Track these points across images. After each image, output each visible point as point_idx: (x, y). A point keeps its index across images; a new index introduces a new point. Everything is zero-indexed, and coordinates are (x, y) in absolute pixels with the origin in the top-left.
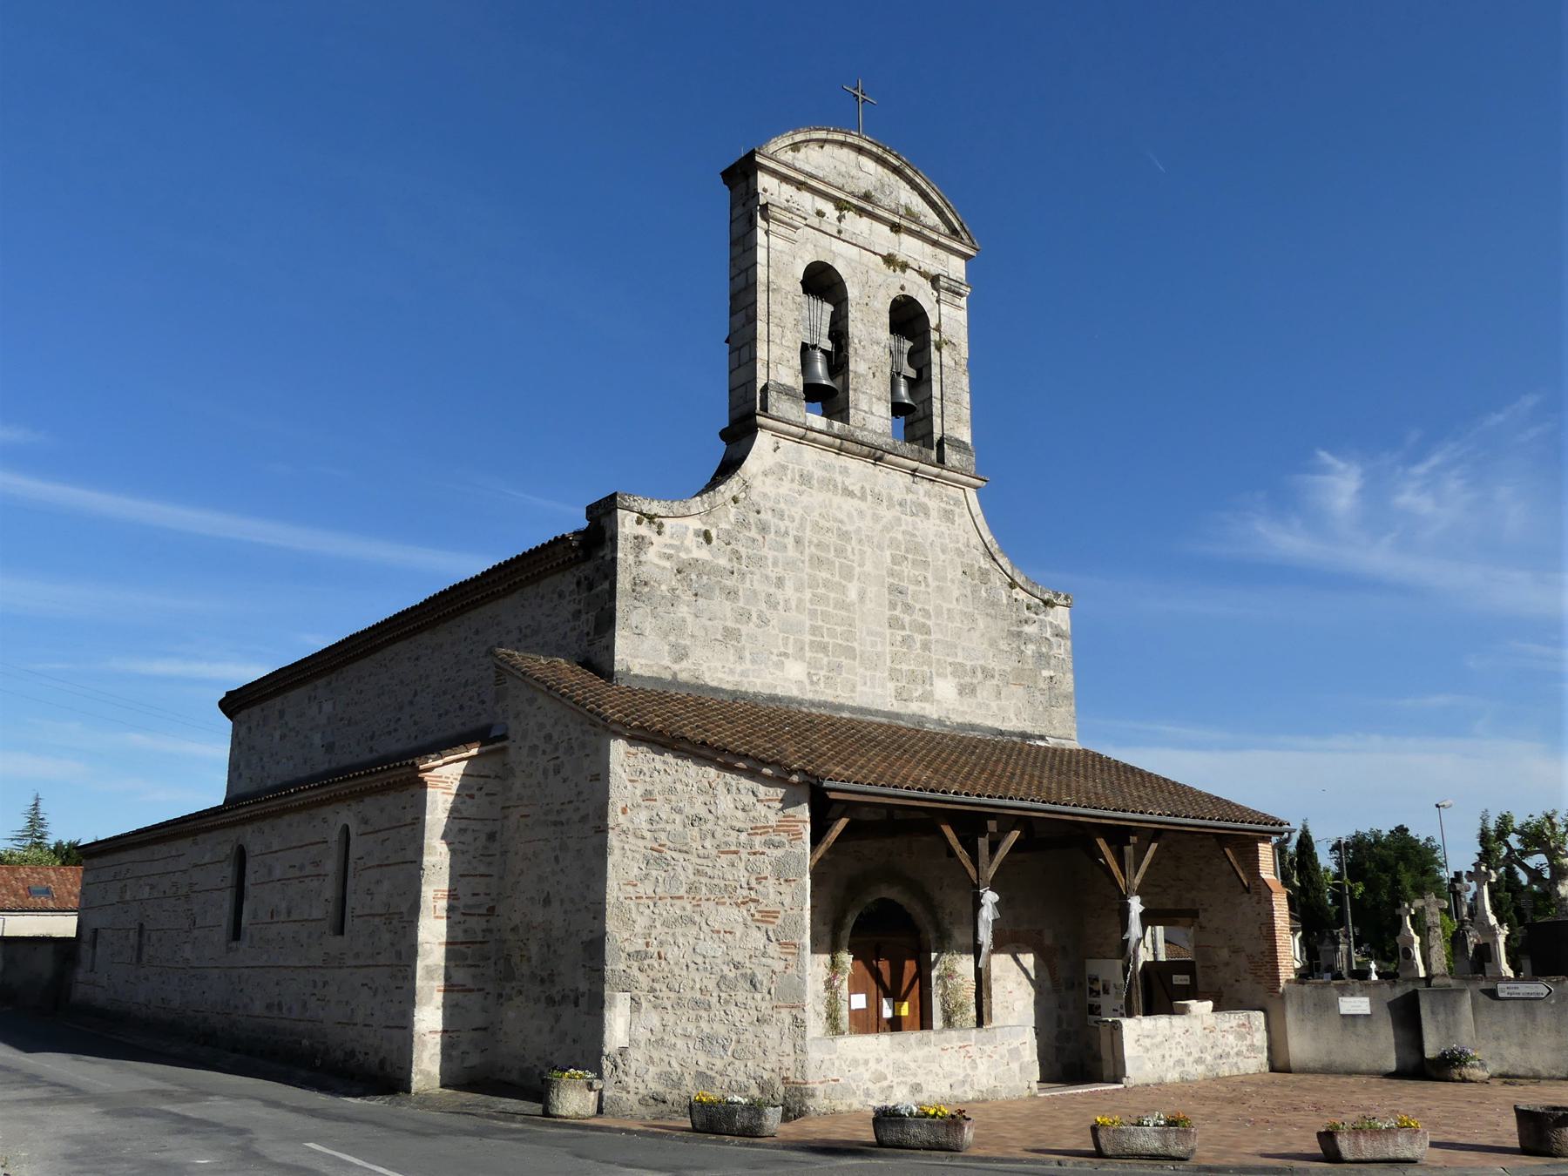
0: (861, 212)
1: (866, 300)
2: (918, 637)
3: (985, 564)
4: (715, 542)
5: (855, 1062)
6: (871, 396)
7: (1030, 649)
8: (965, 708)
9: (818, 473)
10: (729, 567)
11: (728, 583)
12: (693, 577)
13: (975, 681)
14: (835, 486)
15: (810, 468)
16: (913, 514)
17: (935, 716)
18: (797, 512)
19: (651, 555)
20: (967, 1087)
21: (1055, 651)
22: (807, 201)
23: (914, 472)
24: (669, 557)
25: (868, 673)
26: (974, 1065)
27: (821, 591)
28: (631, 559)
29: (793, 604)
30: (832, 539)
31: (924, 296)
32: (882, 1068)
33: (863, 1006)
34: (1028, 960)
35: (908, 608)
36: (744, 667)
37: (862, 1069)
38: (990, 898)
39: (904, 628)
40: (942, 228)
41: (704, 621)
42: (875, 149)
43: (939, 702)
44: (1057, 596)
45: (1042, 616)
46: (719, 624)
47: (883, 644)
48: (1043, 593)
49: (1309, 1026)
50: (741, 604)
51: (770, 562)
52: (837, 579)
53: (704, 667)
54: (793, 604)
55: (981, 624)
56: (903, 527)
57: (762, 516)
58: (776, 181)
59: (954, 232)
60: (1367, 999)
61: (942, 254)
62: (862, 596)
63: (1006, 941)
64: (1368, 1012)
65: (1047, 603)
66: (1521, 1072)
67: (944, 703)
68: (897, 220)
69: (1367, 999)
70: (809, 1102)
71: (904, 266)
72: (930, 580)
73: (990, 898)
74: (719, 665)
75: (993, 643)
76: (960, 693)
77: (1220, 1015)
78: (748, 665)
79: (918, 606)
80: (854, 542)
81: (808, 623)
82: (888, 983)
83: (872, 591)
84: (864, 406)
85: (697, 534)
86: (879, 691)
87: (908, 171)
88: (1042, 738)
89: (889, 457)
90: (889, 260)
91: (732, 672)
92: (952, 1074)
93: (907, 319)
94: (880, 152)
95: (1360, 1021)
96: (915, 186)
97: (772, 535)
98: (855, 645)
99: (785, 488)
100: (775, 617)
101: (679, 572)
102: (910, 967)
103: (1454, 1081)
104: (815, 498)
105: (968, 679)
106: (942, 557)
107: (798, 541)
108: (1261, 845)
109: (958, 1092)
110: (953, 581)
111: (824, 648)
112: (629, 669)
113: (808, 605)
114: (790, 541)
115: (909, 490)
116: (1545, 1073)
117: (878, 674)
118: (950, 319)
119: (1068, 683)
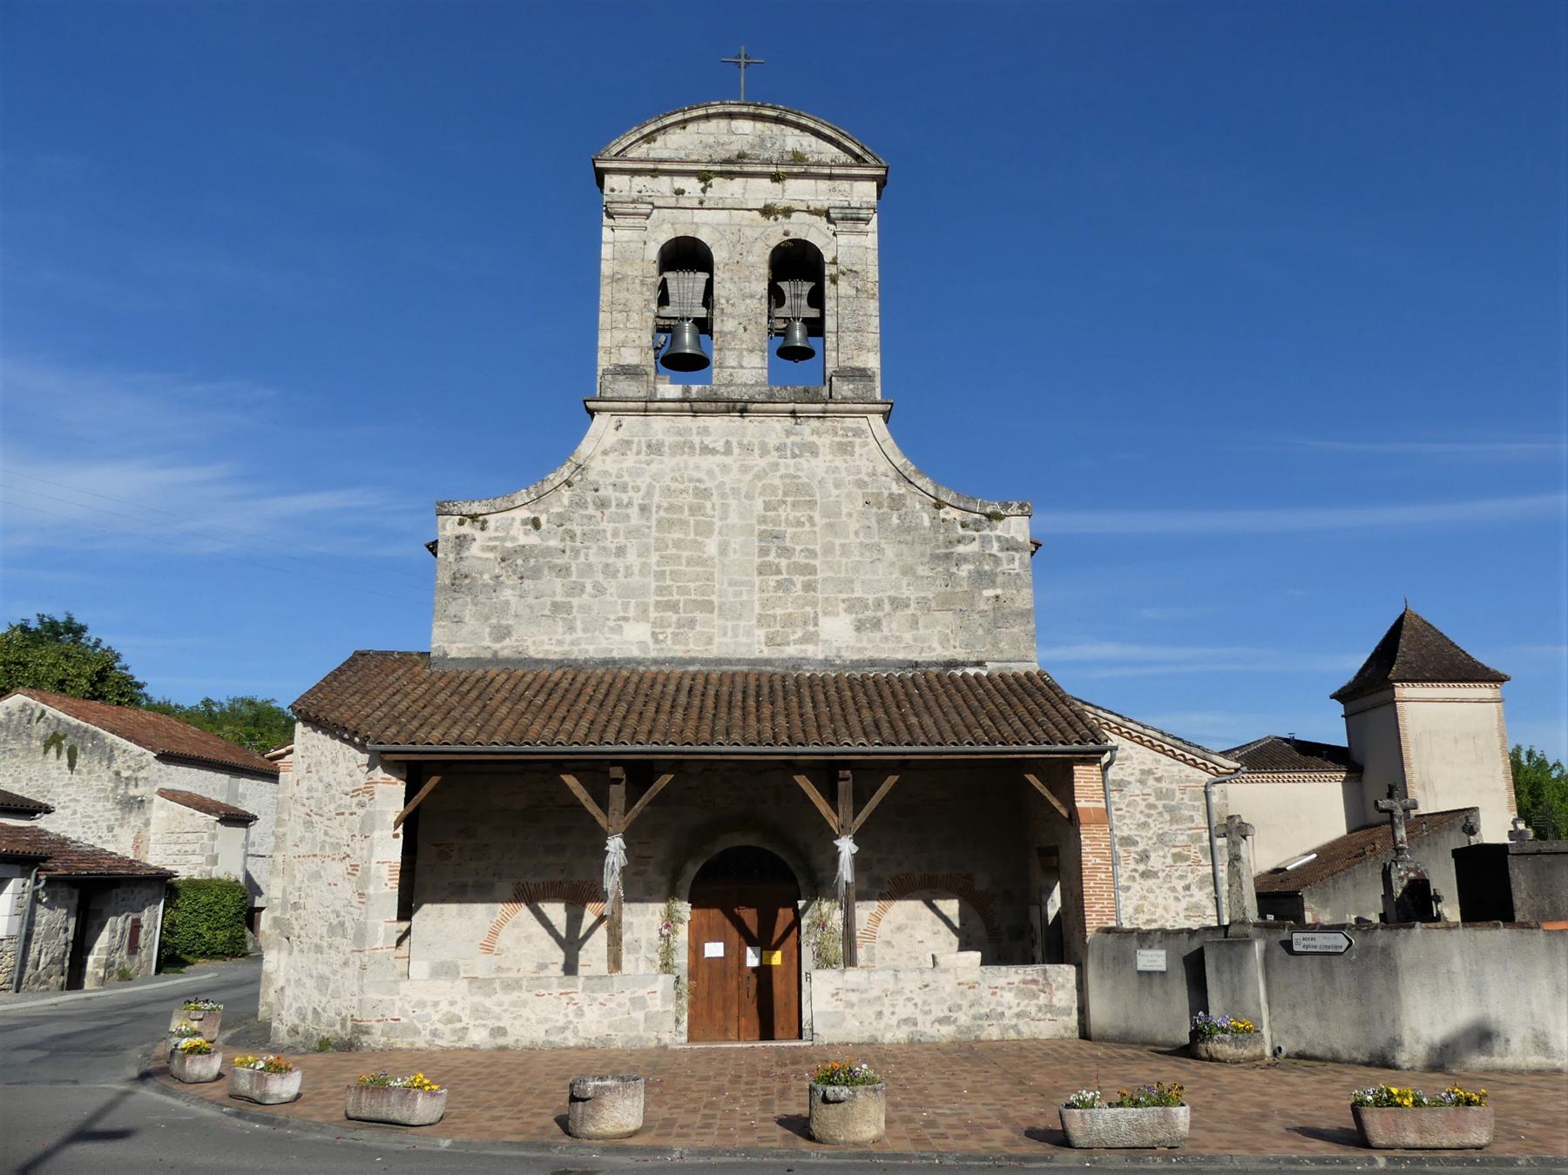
0: (730, 175)
2: (799, 580)
3: (896, 489)
4: (544, 526)
5: (422, 1004)
6: (741, 351)
7: (965, 570)
8: (865, 644)
9: (669, 440)
10: (561, 546)
11: (559, 562)
12: (519, 562)
13: (880, 614)
14: (692, 448)
15: (660, 436)
16: (794, 456)
17: (821, 657)
18: (643, 482)
19: (474, 550)
20: (569, 1034)
21: (1005, 567)
22: (664, 184)
23: (793, 413)
24: (493, 549)
25: (730, 624)
26: (580, 1013)
27: (672, 551)
28: (451, 557)
29: (636, 569)
30: (688, 499)
31: (815, 233)
32: (456, 1010)
33: (721, 954)
34: (951, 907)
35: (785, 551)
36: (575, 636)
37: (430, 1010)
38: (615, 845)
39: (779, 572)
41: (530, 600)
42: (745, 109)
43: (825, 641)
44: (1006, 506)
45: (986, 532)
46: (548, 600)
47: (750, 592)
48: (983, 505)
49: (1109, 983)
50: (574, 578)
51: (609, 535)
52: (692, 536)
53: (529, 643)
54: (636, 569)
55: (890, 553)
56: (782, 471)
57: (601, 493)
58: (626, 178)
59: (857, 157)
60: (1163, 953)
61: (844, 185)
62: (723, 549)
63: (638, 888)
64: (1164, 968)
65: (990, 517)
66: (1318, 1052)
67: (835, 639)
68: (773, 169)
69: (1163, 953)
70: (364, 1038)
72: (817, 518)
73: (615, 845)
74: (546, 638)
75: (907, 571)
76: (858, 629)
77: (992, 970)
78: (580, 634)
79: (798, 548)
80: (715, 498)
81: (654, 585)
82: (754, 931)
83: (736, 542)
84: (731, 360)
85: (524, 522)
86: (743, 639)
87: (791, 117)
88: (979, 664)
89: (750, 406)
90: (767, 211)
91: (560, 643)
92: (546, 1020)
93: (796, 263)
94: (752, 109)
95: (1157, 980)
97: (613, 509)
98: (714, 598)
99: (630, 460)
100: (612, 586)
101: (503, 560)
102: (785, 915)
103: (1202, 1059)
104: (668, 462)
105: (869, 613)
106: (835, 492)
107: (644, 509)
108: (1079, 770)
109: (556, 1039)
110: (850, 515)
111: (673, 607)
112: (445, 654)
113: (655, 568)
114: (634, 511)
115: (788, 433)
116: (1345, 1056)
117: (742, 623)
118: (853, 252)
119: (1024, 598)
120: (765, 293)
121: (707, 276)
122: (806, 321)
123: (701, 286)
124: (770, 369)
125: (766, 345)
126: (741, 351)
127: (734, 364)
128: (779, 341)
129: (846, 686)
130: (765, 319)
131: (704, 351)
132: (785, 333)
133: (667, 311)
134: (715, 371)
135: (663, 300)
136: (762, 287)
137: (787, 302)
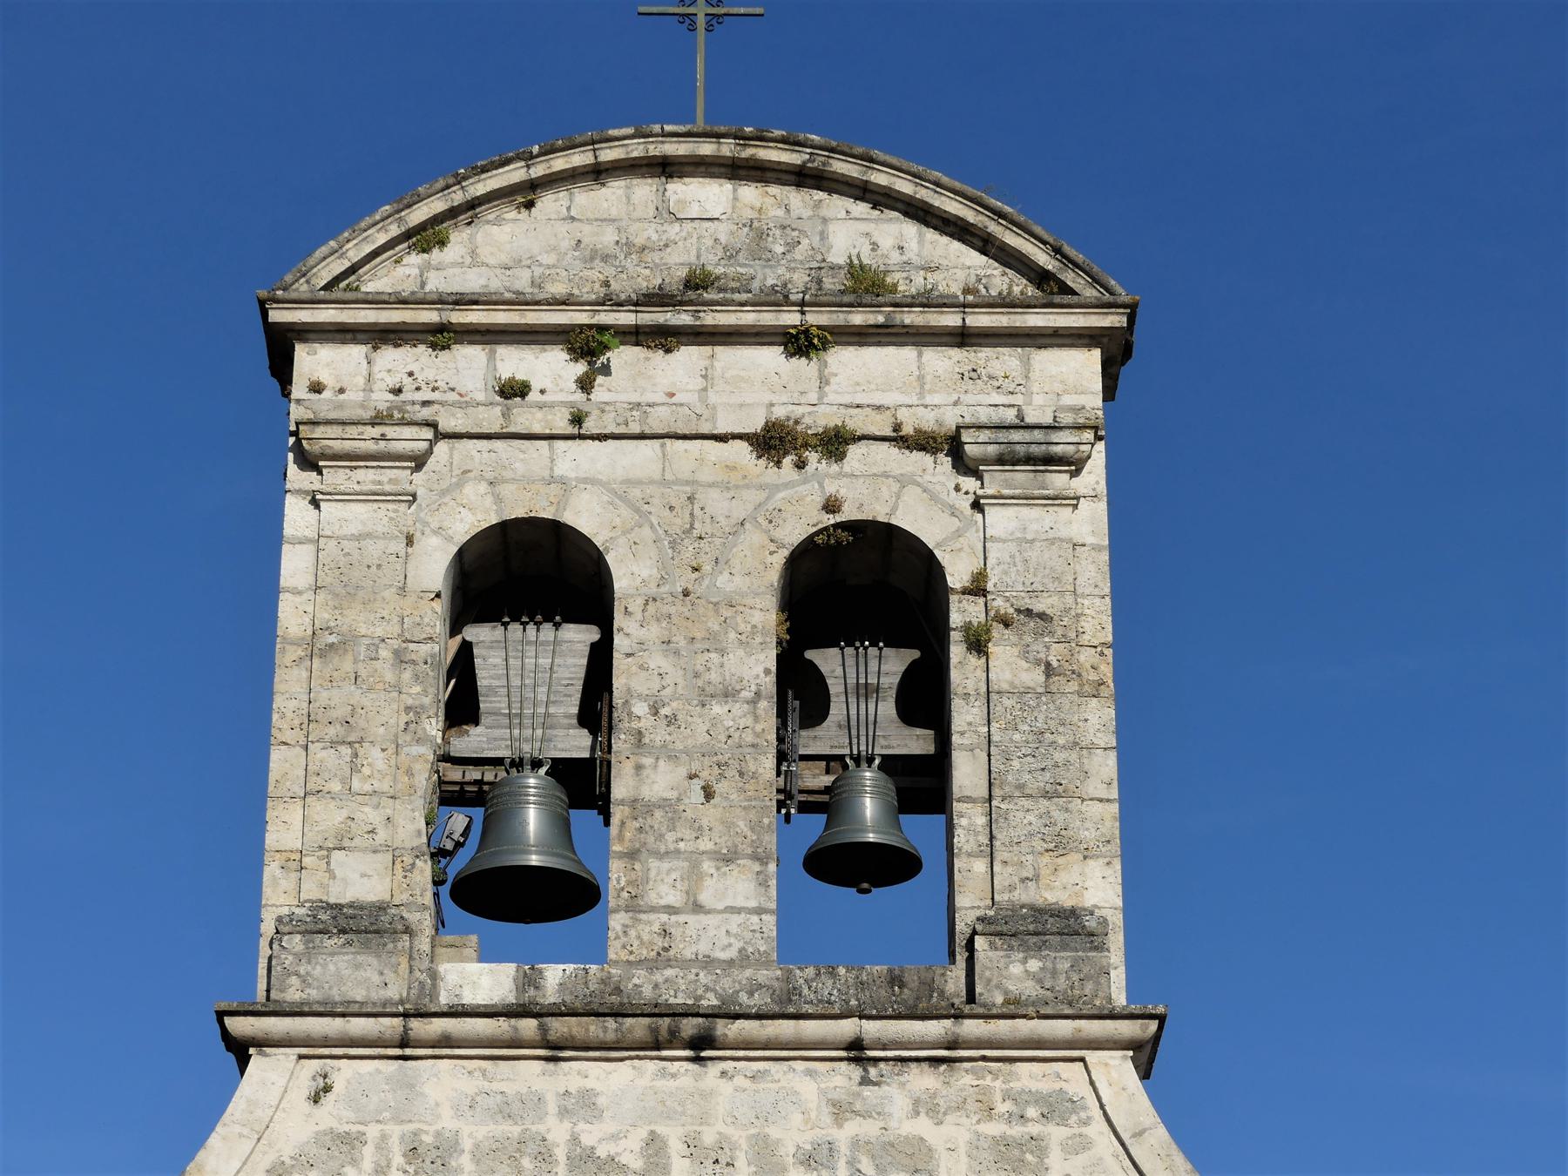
1: (685, 579)
6: (694, 859)
15: (448, 1122)
22: (469, 367)
23: (856, 1050)
31: (917, 501)
40: (1000, 280)
42: (707, 148)
58: (356, 353)
59: (1042, 278)
61: (1005, 360)
68: (791, 318)
71: (835, 443)
87: (841, 167)
90: (774, 441)
94: (727, 148)
96: (881, 199)
115: (841, 1111)
118: (1035, 557)
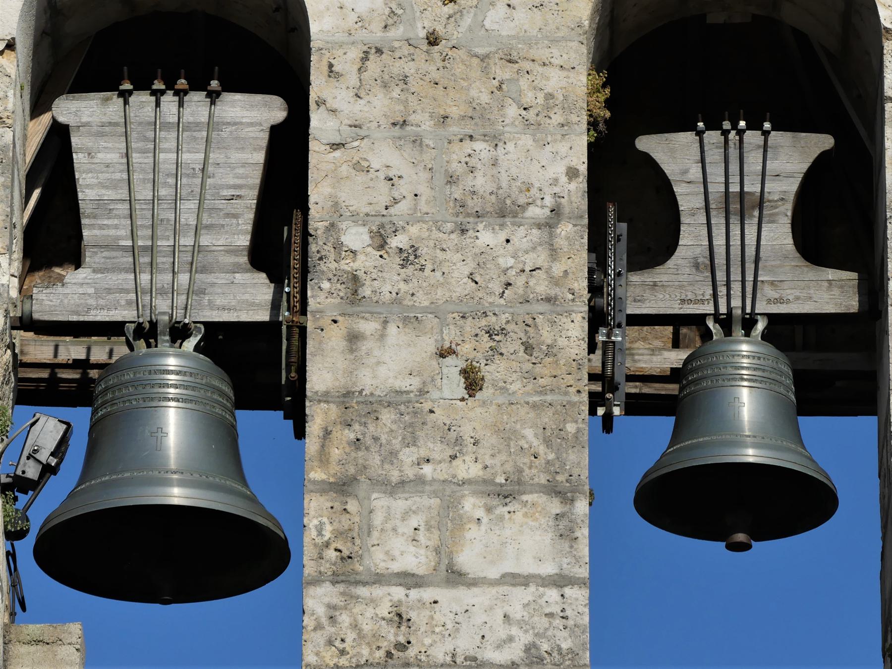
6: (450, 493)
84: (399, 542)
120: (576, 193)
121: (269, 110)
122: (785, 331)
123: (243, 166)
124: (600, 584)
125: (578, 462)
126: (450, 493)
127: (413, 559)
128: (649, 441)
129: (336, 578)
130: (576, 328)
131: (267, 504)
132: (678, 399)
133: (71, 294)
134: (317, 600)
135: (53, 238)
136: (556, 164)
137: (691, 239)
